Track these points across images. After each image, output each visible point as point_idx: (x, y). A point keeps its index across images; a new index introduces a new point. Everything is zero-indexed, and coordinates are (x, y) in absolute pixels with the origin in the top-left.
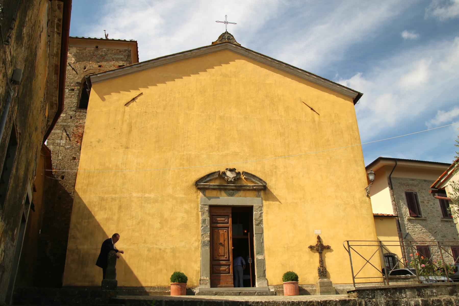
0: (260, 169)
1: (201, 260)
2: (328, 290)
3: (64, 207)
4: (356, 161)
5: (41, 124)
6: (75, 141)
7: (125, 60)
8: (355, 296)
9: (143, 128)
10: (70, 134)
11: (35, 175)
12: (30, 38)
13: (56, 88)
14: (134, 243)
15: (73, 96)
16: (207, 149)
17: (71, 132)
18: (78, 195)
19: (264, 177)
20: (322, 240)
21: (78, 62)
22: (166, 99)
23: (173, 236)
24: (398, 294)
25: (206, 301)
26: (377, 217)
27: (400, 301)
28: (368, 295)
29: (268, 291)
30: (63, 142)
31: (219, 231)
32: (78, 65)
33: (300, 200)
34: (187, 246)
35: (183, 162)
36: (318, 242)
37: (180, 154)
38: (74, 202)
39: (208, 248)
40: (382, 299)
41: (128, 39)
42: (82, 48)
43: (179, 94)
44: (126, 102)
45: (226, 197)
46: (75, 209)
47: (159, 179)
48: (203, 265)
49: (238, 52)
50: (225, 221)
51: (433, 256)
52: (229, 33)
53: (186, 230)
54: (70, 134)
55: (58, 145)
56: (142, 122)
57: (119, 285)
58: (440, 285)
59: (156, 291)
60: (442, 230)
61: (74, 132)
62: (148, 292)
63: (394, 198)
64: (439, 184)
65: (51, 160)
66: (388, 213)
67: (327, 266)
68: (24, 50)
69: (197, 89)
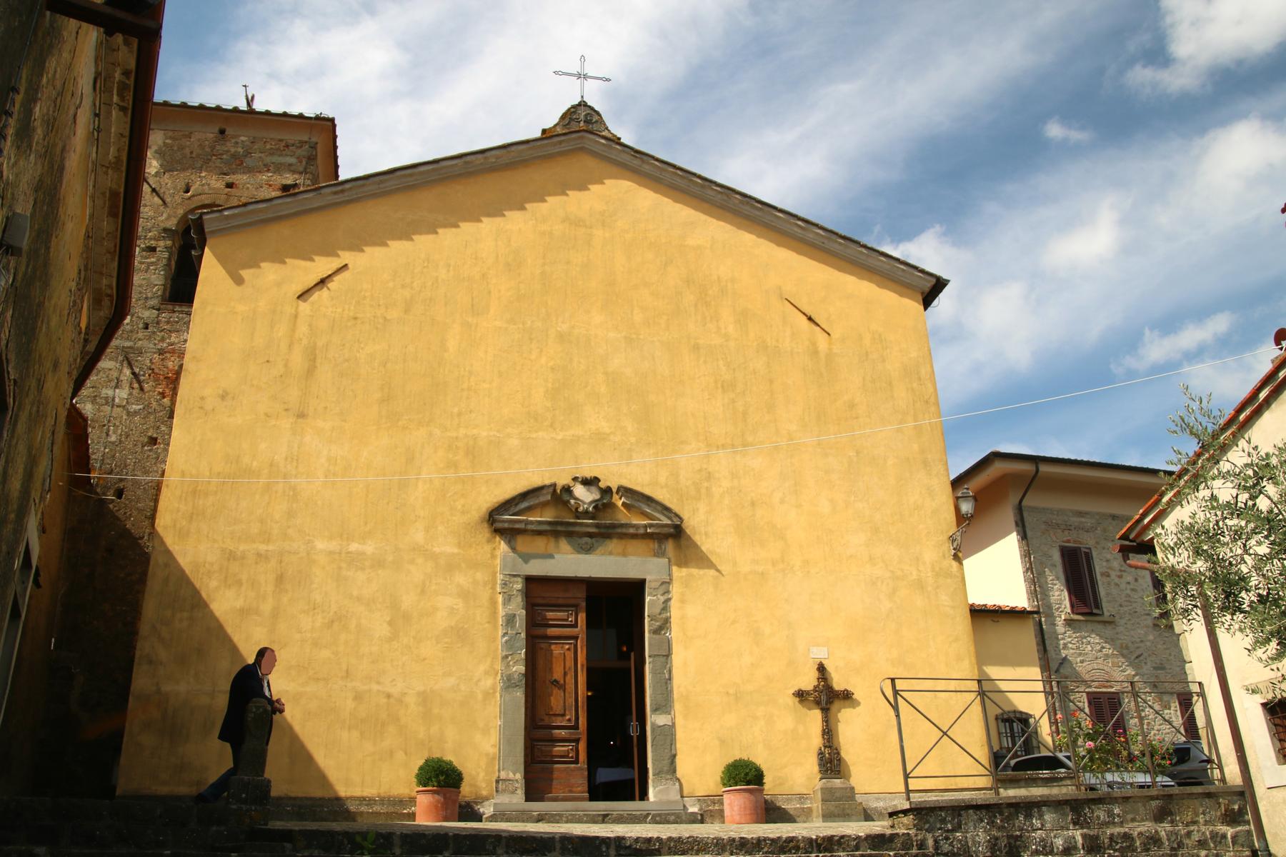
0: (667, 479)
1: (500, 726)
2: (844, 809)
3: (122, 575)
4: (926, 463)
5: (68, 352)
6: (155, 391)
7: (301, 169)
8: (909, 825)
9: (347, 360)
10: (142, 373)
11: (49, 490)
12: (50, 128)
13: (110, 253)
14: (318, 679)
15: (152, 268)
16: (522, 423)
17: (146, 368)
18: (163, 543)
19: (675, 500)
20: (830, 674)
21: (170, 171)
22: (412, 282)
23: (424, 659)
24: (1021, 818)
25: (510, 836)
26: (981, 614)
27: (1028, 838)
28: (943, 821)
29: (682, 811)
30: (122, 394)
31: (550, 646)
32: (166, 179)
33: (774, 565)
34: (463, 687)
35: (456, 458)
36: (818, 679)
37: (449, 434)
38: (152, 563)
39: (520, 695)
40: (980, 834)
41: (309, 113)
42: (182, 133)
43: (448, 271)
44: (300, 289)
45: (572, 556)
46: (154, 584)
47: (388, 503)
48: (506, 740)
49: (612, 159)
50: (567, 620)
51: (1131, 721)
52: (589, 104)
53: (459, 645)
54: (142, 373)
55: (107, 403)
56: (344, 345)
57: (274, 793)
58: (1132, 795)
59: (374, 809)
60: (1154, 649)
61: (153, 367)
62: (354, 812)
63: (1031, 564)
64: (1138, 528)
65: (89, 445)
66: (1012, 604)
67: (841, 745)
68: (35, 160)
69: (497, 257)
